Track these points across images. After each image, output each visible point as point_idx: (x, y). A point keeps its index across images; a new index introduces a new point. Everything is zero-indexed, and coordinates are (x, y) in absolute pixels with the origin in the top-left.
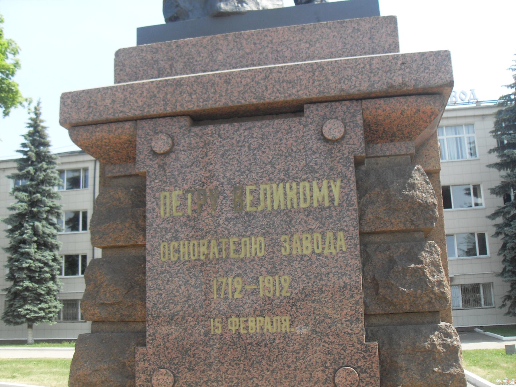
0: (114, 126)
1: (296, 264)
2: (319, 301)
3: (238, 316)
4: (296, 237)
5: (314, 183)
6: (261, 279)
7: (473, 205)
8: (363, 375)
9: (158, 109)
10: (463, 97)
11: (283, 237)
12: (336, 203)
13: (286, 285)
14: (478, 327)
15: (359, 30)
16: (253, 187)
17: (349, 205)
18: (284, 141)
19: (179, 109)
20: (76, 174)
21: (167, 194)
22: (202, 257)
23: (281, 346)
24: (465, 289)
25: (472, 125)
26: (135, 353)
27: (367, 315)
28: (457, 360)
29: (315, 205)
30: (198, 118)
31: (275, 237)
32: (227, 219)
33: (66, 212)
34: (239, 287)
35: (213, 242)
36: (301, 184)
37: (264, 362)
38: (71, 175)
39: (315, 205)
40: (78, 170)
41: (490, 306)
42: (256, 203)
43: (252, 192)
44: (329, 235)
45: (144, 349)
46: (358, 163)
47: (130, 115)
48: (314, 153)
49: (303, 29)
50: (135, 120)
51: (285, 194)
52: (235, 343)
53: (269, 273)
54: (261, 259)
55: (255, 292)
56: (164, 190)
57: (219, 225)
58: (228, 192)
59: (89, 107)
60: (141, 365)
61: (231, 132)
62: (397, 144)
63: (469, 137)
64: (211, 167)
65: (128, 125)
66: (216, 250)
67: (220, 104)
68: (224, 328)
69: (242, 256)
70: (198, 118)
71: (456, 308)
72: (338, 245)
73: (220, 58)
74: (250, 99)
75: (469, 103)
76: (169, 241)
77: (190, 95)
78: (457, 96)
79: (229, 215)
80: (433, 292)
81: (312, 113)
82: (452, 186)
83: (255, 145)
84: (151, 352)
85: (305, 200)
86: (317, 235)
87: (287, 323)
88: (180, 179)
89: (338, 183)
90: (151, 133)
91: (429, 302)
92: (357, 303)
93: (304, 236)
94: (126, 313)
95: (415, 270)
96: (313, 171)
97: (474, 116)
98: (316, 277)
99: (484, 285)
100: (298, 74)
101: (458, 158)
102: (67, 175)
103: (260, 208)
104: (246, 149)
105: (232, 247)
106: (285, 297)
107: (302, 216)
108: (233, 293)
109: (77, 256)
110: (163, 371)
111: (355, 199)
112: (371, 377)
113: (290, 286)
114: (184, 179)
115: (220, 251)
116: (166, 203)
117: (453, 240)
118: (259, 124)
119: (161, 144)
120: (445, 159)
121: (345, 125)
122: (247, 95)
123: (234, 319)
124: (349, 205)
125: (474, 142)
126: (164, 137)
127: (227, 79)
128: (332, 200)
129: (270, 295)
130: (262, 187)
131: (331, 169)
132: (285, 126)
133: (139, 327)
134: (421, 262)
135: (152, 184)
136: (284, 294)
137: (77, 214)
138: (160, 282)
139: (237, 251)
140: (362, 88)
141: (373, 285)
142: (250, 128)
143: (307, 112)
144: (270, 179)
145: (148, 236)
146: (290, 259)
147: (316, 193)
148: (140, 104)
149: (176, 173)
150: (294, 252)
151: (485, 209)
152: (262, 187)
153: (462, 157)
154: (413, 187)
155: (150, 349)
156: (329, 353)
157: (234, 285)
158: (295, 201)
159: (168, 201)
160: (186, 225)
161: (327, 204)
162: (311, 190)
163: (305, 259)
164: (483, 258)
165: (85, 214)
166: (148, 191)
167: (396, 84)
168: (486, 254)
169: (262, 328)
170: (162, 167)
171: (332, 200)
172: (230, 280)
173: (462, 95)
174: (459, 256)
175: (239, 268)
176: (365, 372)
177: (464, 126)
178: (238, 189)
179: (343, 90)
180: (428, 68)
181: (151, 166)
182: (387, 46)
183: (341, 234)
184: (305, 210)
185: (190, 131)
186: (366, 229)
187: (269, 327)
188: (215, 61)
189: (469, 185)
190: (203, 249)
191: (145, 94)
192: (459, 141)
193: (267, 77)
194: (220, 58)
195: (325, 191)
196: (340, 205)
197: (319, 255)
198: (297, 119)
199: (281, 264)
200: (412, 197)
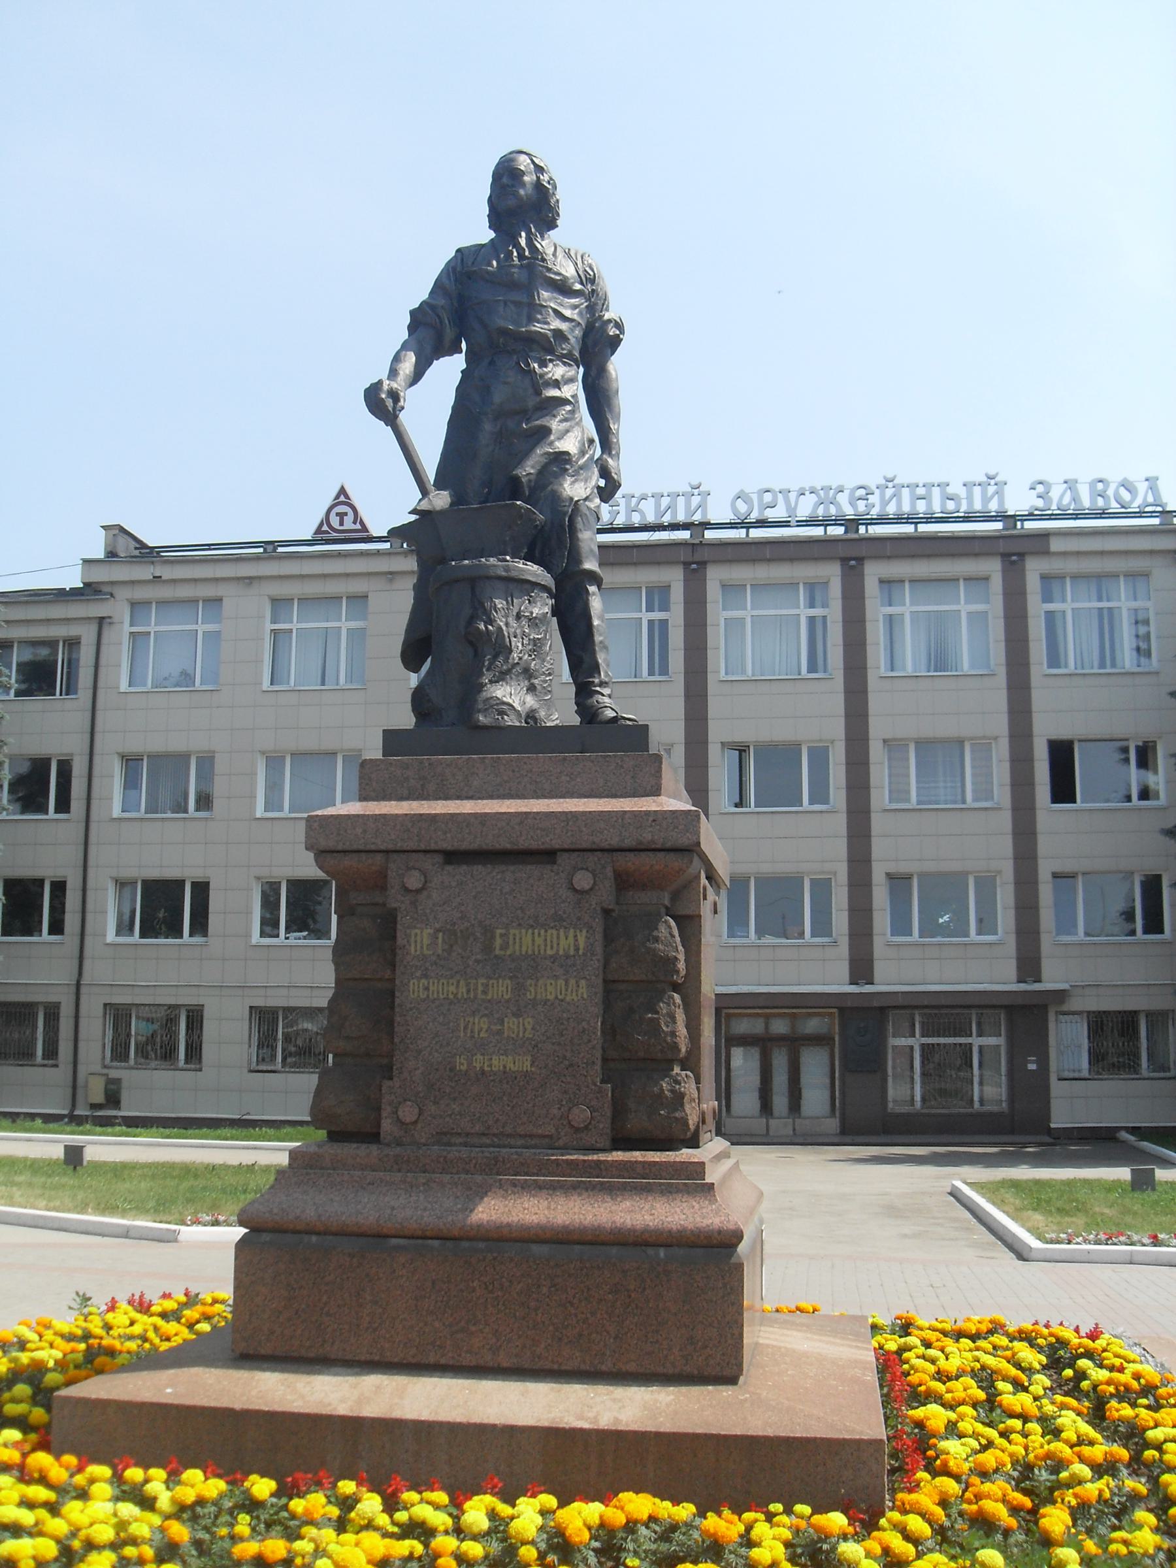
0: (363, 856)
1: (540, 1008)
2: (559, 1044)
3: (483, 1054)
4: (541, 982)
5: (562, 931)
7: (1135, 796)
8: (595, 1114)
10: (1126, 496)
11: (529, 982)
12: (581, 952)
13: (529, 1027)
14: (1127, 1129)
15: (622, 767)
16: (503, 931)
17: (592, 954)
19: (433, 847)
20: (44, 652)
21: (418, 931)
22: (451, 996)
24: (1098, 1023)
25: (1146, 575)
26: (381, 1086)
27: (605, 1060)
28: (682, 1105)
29: (561, 952)
30: (453, 857)
31: (521, 980)
32: (477, 961)
33: (12, 758)
34: (485, 1027)
35: (462, 983)
36: (549, 932)
38: (28, 655)
39: (561, 952)
40: (52, 644)
41: (1162, 1075)
42: (504, 947)
43: (502, 935)
44: (572, 982)
45: (390, 1083)
46: (607, 912)
47: (383, 848)
48: (564, 902)
50: (387, 852)
51: (533, 941)
53: (515, 1015)
54: (508, 1001)
55: (500, 1032)
56: (415, 927)
57: (468, 966)
58: (478, 935)
59: (339, 834)
63: (1136, 610)
64: (463, 908)
65: (379, 858)
66: (464, 990)
68: (470, 1064)
69: (489, 997)
70: (453, 857)
71: (1071, 1075)
72: (579, 993)
75: (1140, 514)
76: (419, 979)
78: (1110, 493)
79: (479, 957)
80: (665, 1041)
82: (1080, 741)
83: (507, 889)
84: (397, 1085)
85: (552, 948)
86: (561, 982)
87: (528, 1063)
89: (584, 931)
91: (662, 1051)
92: (594, 1048)
93: (549, 982)
95: (652, 1020)
96: (562, 919)
97: (1152, 553)
99: (1149, 1014)
101: (1102, 665)
102: (18, 656)
103: (508, 953)
105: (480, 988)
107: (548, 963)
108: (480, 1031)
109: (40, 882)
110: (409, 1103)
111: (599, 949)
115: (468, 991)
116: (418, 940)
117: (1074, 890)
118: (512, 868)
119: (414, 881)
120: (1066, 666)
121: (595, 876)
123: (479, 1057)
124: (592, 954)
125: (1146, 622)
126: (416, 873)
128: (577, 949)
130: (512, 931)
131: (579, 919)
133: (385, 1061)
134: (657, 1013)
135: (403, 921)
136: (527, 1035)
137: (40, 766)
139: (484, 992)
141: (610, 1031)
142: (503, 872)
144: (520, 925)
145: (398, 972)
146: (534, 1003)
147: (563, 942)
149: (428, 911)
150: (539, 997)
151: (1165, 809)
152: (512, 931)
153: (1114, 665)
154: (657, 939)
155: (396, 1082)
156: (565, 1092)
157: (481, 1025)
158: (543, 947)
159: (419, 939)
160: (436, 964)
161: (572, 952)
162: (558, 938)
164: (1153, 943)
166: (399, 927)
168: (1161, 931)
169: (505, 1067)
170: (414, 903)
171: (577, 949)
172: (476, 1021)
173: (1122, 491)
174: (1087, 934)
175: (486, 1008)
177: (1122, 578)
178: (489, 932)
181: (402, 902)
182: (649, 787)
183: (583, 983)
184: (551, 957)
189: (1127, 740)
190: (452, 989)
191: (398, 827)
192: (1107, 620)
193: (521, 823)
194: (475, 783)
195: (571, 939)
196: (584, 954)
198: (549, 867)
200: (654, 950)
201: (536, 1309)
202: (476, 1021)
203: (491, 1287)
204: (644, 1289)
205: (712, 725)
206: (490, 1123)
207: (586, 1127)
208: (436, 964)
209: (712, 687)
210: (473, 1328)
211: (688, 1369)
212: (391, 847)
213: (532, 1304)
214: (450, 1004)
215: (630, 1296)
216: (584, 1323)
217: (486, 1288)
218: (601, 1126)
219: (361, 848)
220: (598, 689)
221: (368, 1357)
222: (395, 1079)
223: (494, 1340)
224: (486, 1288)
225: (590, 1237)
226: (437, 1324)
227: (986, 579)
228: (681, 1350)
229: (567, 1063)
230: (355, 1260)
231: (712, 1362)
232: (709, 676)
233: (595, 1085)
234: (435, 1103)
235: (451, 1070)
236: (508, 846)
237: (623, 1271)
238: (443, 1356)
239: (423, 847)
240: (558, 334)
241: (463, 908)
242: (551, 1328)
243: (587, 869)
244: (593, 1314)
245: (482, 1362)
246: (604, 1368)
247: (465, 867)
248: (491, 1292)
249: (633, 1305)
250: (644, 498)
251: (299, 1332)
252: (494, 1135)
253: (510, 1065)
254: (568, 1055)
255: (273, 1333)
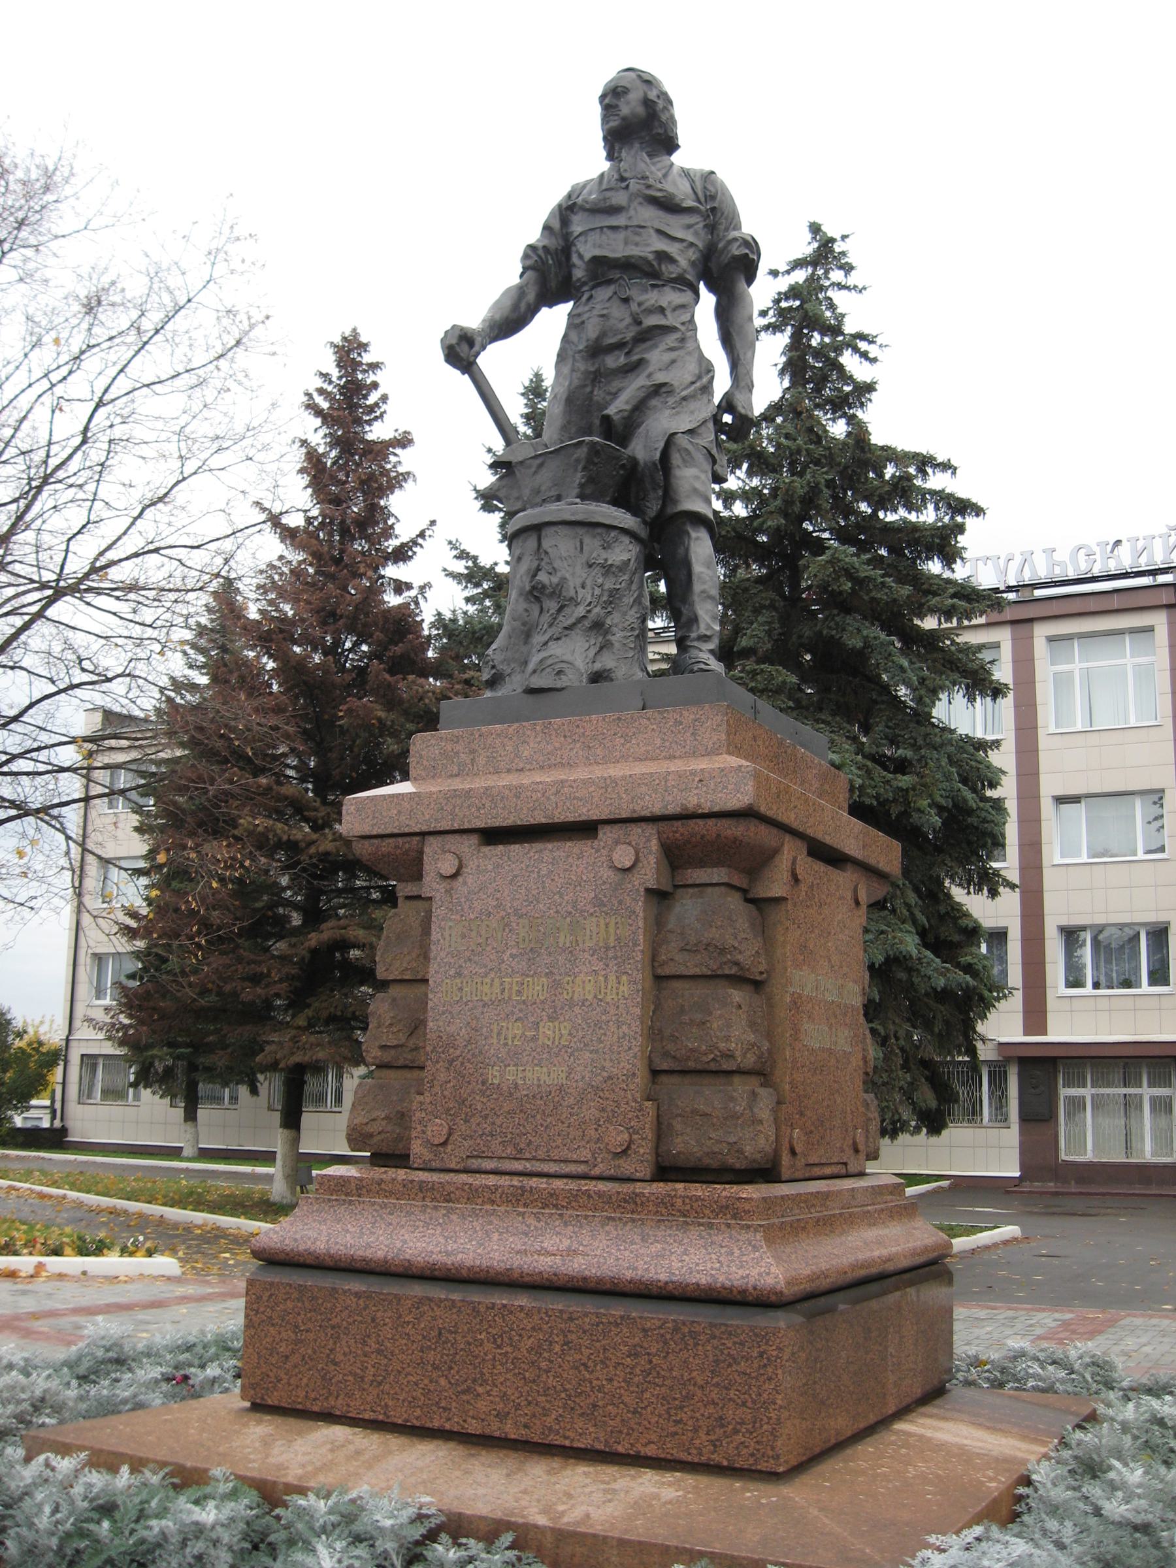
1: (577, 1010)
2: (597, 1052)
6: (541, 1024)
8: (635, 1137)
9: (444, 825)
15: (681, 723)
18: (574, 868)
23: (556, 1099)
30: (493, 836)
31: (558, 978)
34: (519, 1032)
35: (497, 982)
37: (539, 1117)
45: (420, 1098)
49: (619, 719)
50: (423, 834)
52: (511, 1094)
55: (534, 1039)
59: (374, 818)
60: (418, 1114)
61: (521, 854)
62: (709, 870)
66: (498, 991)
67: (509, 822)
70: (493, 836)
73: (526, 753)
74: (540, 818)
77: (479, 809)
79: (514, 951)
81: (606, 835)
88: (466, 907)
90: (439, 851)
94: (409, 1057)
98: (595, 1025)
100: (591, 789)
104: (535, 875)
106: (564, 1046)
112: (643, 1139)
113: (570, 1034)
114: (470, 907)
118: (550, 846)
122: (536, 813)
126: (450, 856)
127: (518, 791)
129: (549, 1043)
132: (576, 850)
138: (441, 1024)
139: (519, 992)
140: (654, 810)
143: (600, 834)
148: (427, 817)
149: (463, 900)
150: (575, 998)
156: (603, 1110)
160: (470, 960)
163: (587, 1003)
165: (1075, 982)
166: (433, 919)
167: (690, 806)
172: (510, 1026)
175: (520, 1011)
176: (638, 1133)
179: (635, 811)
180: (726, 788)
185: (479, 851)
186: (660, 971)
187: (546, 1078)
188: (520, 757)
193: (558, 792)
194: (526, 753)
197: (601, 1000)
198: (589, 843)
199: (562, 1008)
201: (547, 1371)
202: (510, 1026)
203: (499, 1341)
204: (668, 1353)
205: (1043, 778)
206: (522, 1146)
207: (624, 1152)
208: (470, 960)
209: (1043, 742)
210: (480, 1390)
211: (717, 1458)
212: (425, 828)
213: (544, 1365)
214: (484, 1006)
215: (650, 1362)
216: (599, 1391)
217: (495, 1341)
218: (642, 1151)
219: (396, 831)
220: (696, 644)
221: (372, 1416)
222: (427, 1094)
223: (502, 1405)
224: (495, 1341)
225: (592, 1285)
226: (443, 1382)
227: (1151, 629)
228: (708, 1434)
229: (605, 1074)
230: (361, 1302)
231: (745, 1451)
232: (1040, 730)
233: (635, 1101)
234: (466, 1121)
235: (483, 1083)
236: (544, 821)
237: (644, 1330)
238: (449, 1419)
239: (456, 826)
240: (663, 256)
241: (499, 895)
242: (563, 1395)
243: (629, 844)
244: (610, 1380)
245: (487, 1431)
246: (621, 1449)
247: (501, 847)
248: (499, 1347)
249: (654, 1374)
250: (1118, 543)
251: (305, 1380)
252: (527, 1159)
253: (544, 1078)
254: (608, 1064)
255: (279, 1381)
